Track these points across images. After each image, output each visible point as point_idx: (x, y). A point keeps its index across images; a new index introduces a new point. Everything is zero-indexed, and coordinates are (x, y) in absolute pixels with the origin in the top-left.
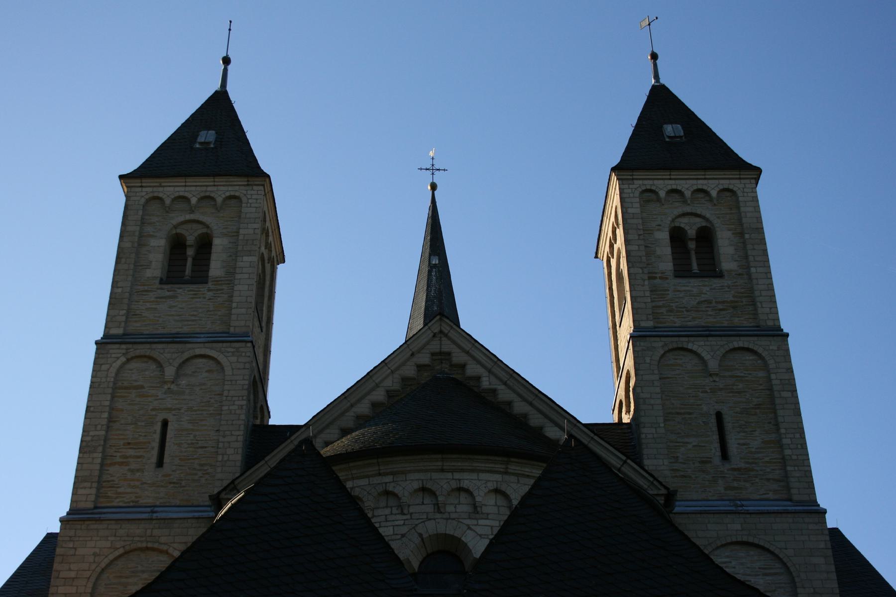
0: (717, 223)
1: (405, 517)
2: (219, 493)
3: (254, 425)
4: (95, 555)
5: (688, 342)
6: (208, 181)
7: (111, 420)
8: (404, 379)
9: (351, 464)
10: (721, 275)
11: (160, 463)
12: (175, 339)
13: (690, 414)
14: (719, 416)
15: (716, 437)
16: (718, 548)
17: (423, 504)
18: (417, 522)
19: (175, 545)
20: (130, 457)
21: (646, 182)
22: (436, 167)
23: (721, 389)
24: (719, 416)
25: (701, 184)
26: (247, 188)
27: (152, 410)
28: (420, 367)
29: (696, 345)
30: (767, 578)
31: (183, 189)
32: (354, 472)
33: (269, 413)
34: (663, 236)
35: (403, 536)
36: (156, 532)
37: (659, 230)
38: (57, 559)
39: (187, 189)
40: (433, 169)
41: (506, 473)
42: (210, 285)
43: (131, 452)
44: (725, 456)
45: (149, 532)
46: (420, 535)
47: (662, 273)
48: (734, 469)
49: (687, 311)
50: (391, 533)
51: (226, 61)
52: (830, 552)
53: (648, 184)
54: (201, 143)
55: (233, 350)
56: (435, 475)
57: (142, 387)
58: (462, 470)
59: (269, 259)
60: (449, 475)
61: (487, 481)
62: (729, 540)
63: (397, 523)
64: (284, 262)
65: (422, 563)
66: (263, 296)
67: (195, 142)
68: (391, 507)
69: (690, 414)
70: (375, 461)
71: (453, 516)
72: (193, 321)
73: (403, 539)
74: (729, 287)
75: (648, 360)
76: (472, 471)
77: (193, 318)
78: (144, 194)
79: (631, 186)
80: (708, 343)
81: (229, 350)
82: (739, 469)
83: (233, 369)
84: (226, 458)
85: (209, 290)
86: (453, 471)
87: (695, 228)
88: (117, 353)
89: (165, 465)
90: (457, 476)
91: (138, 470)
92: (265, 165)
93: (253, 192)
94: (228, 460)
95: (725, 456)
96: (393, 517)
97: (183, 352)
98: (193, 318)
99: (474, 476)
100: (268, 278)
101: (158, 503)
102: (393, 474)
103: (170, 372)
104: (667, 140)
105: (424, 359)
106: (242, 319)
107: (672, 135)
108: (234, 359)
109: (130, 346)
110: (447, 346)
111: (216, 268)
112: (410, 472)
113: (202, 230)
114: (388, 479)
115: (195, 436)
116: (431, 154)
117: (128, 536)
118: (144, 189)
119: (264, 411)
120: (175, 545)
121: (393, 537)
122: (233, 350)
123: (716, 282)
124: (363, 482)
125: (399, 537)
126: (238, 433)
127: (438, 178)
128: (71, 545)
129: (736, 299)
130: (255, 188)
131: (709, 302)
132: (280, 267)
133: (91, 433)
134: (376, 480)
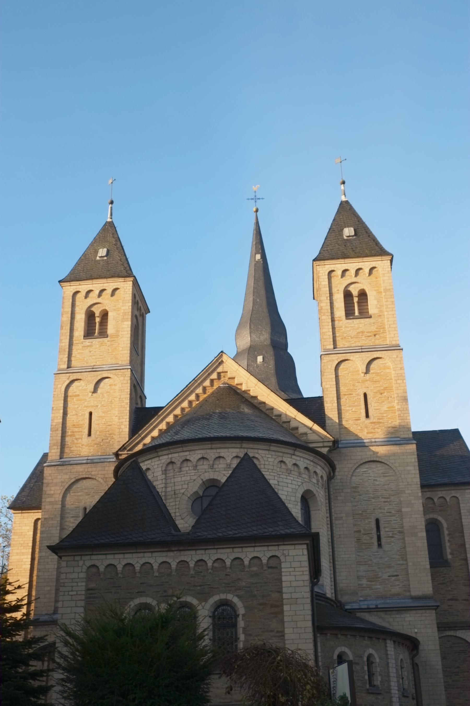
1: (195, 471)
2: (117, 451)
3: (137, 408)
4: (62, 482)
5: (350, 356)
6: (104, 281)
9: (170, 447)
10: (370, 317)
11: (90, 434)
13: (351, 394)
14: (365, 395)
16: (356, 469)
17: (203, 464)
18: (201, 473)
19: (99, 476)
20: (76, 432)
21: (331, 266)
22: (258, 197)
23: (367, 380)
24: (365, 395)
26: (124, 283)
27: (84, 407)
30: (386, 478)
31: (91, 286)
32: (172, 450)
33: (145, 397)
35: (194, 480)
36: (90, 470)
37: (338, 293)
38: (45, 485)
39: (94, 285)
40: (255, 199)
41: (241, 448)
42: (108, 339)
43: (76, 430)
44: (367, 416)
45: (86, 470)
46: (202, 480)
47: (339, 317)
48: (372, 423)
49: (351, 338)
50: (189, 479)
52: (417, 464)
54: (100, 257)
55: (121, 373)
56: (208, 451)
57: (78, 395)
58: (220, 448)
59: (140, 315)
60: (215, 451)
61: (232, 452)
62: (367, 460)
63: (192, 474)
64: (149, 312)
65: (204, 492)
66: (138, 336)
67: (96, 256)
68: (189, 467)
69: (351, 394)
70: (180, 445)
71: (217, 470)
72: (101, 358)
73: (195, 482)
74: (374, 323)
75: (329, 367)
76: (225, 448)
77: (101, 357)
78: (72, 290)
79: (324, 269)
80: (361, 356)
81: (119, 373)
82: (374, 423)
83: (122, 384)
84: (121, 430)
85: (108, 341)
86: (216, 449)
87: (358, 290)
89: (92, 435)
90: (218, 451)
91: (79, 438)
93: (127, 285)
94: (122, 431)
96: (190, 472)
97: (97, 376)
98: (101, 357)
99: (226, 450)
100: (140, 327)
101: (90, 455)
102: (189, 451)
104: (345, 238)
107: (348, 235)
108: (122, 378)
109: (71, 374)
111: (111, 329)
112: (196, 450)
114: (187, 453)
115: (106, 420)
116: (255, 188)
117: (76, 472)
118: (72, 287)
119: (142, 398)
120: (99, 476)
121: (190, 481)
122: (121, 373)
124: (176, 455)
125: (193, 481)
126: (125, 417)
127: (259, 204)
128: (50, 478)
129: (377, 330)
130: (128, 282)
131: (362, 332)
132: (148, 316)
133: (56, 421)
134: (182, 454)
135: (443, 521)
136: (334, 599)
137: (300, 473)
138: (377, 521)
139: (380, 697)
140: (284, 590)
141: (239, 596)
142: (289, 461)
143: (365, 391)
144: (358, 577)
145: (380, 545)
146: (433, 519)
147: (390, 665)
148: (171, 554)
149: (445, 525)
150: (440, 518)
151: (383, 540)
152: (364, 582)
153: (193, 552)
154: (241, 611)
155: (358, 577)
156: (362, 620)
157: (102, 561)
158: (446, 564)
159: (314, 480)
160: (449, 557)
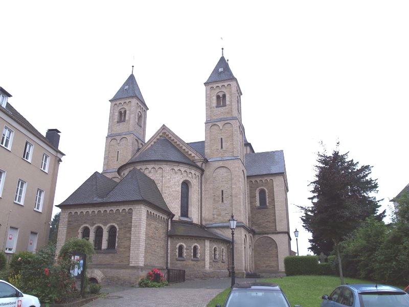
0: (226, 93)
7: (109, 152)
8: (157, 139)
11: (117, 160)
12: (119, 135)
14: (222, 139)
15: (220, 144)
24: (222, 139)
25: (223, 84)
28: (161, 136)
29: (218, 123)
34: (215, 98)
44: (222, 148)
51: (223, 49)
53: (212, 86)
88: (110, 139)
92: (235, 73)
95: (222, 148)
103: (118, 141)
105: (161, 134)
106: (235, 114)
110: (165, 131)
113: (223, 93)
123: (224, 108)
135: (266, 190)
136: (199, 224)
137: (182, 174)
138: (222, 191)
139: (199, 262)
140: (133, 222)
141: (117, 224)
142: (176, 169)
143: (222, 137)
144: (213, 215)
145: (223, 201)
146: (262, 189)
147: (206, 250)
148: (95, 208)
149: (267, 191)
150: (265, 188)
151: (224, 199)
152: (215, 216)
153: (115, 207)
154: (118, 230)
155: (213, 215)
156: (212, 234)
157: (73, 211)
158: (266, 208)
159: (190, 176)
160: (268, 204)
